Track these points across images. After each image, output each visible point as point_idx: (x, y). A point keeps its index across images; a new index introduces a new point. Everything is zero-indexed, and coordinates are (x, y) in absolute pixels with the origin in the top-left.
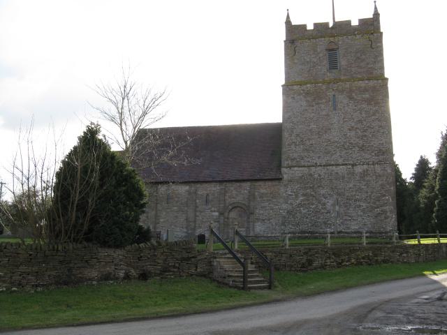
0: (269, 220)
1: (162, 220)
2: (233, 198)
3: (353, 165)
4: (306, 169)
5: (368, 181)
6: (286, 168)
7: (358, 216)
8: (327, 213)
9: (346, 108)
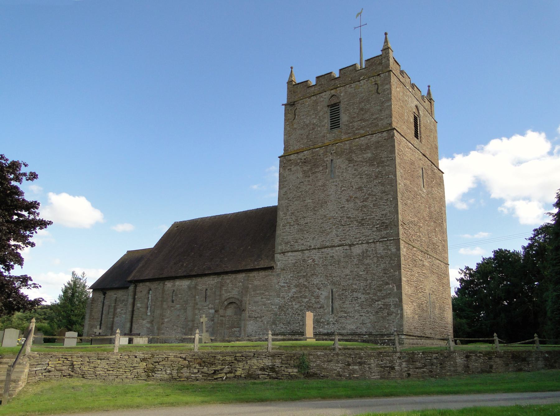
0: (261, 318)
1: (166, 320)
2: (230, 292)
3: (350, 246)
4: (300, 253)
5: (368, 264)
6: (280, 253)
7: (355, 311)
8: (320, 308)
9: (345, 174)
